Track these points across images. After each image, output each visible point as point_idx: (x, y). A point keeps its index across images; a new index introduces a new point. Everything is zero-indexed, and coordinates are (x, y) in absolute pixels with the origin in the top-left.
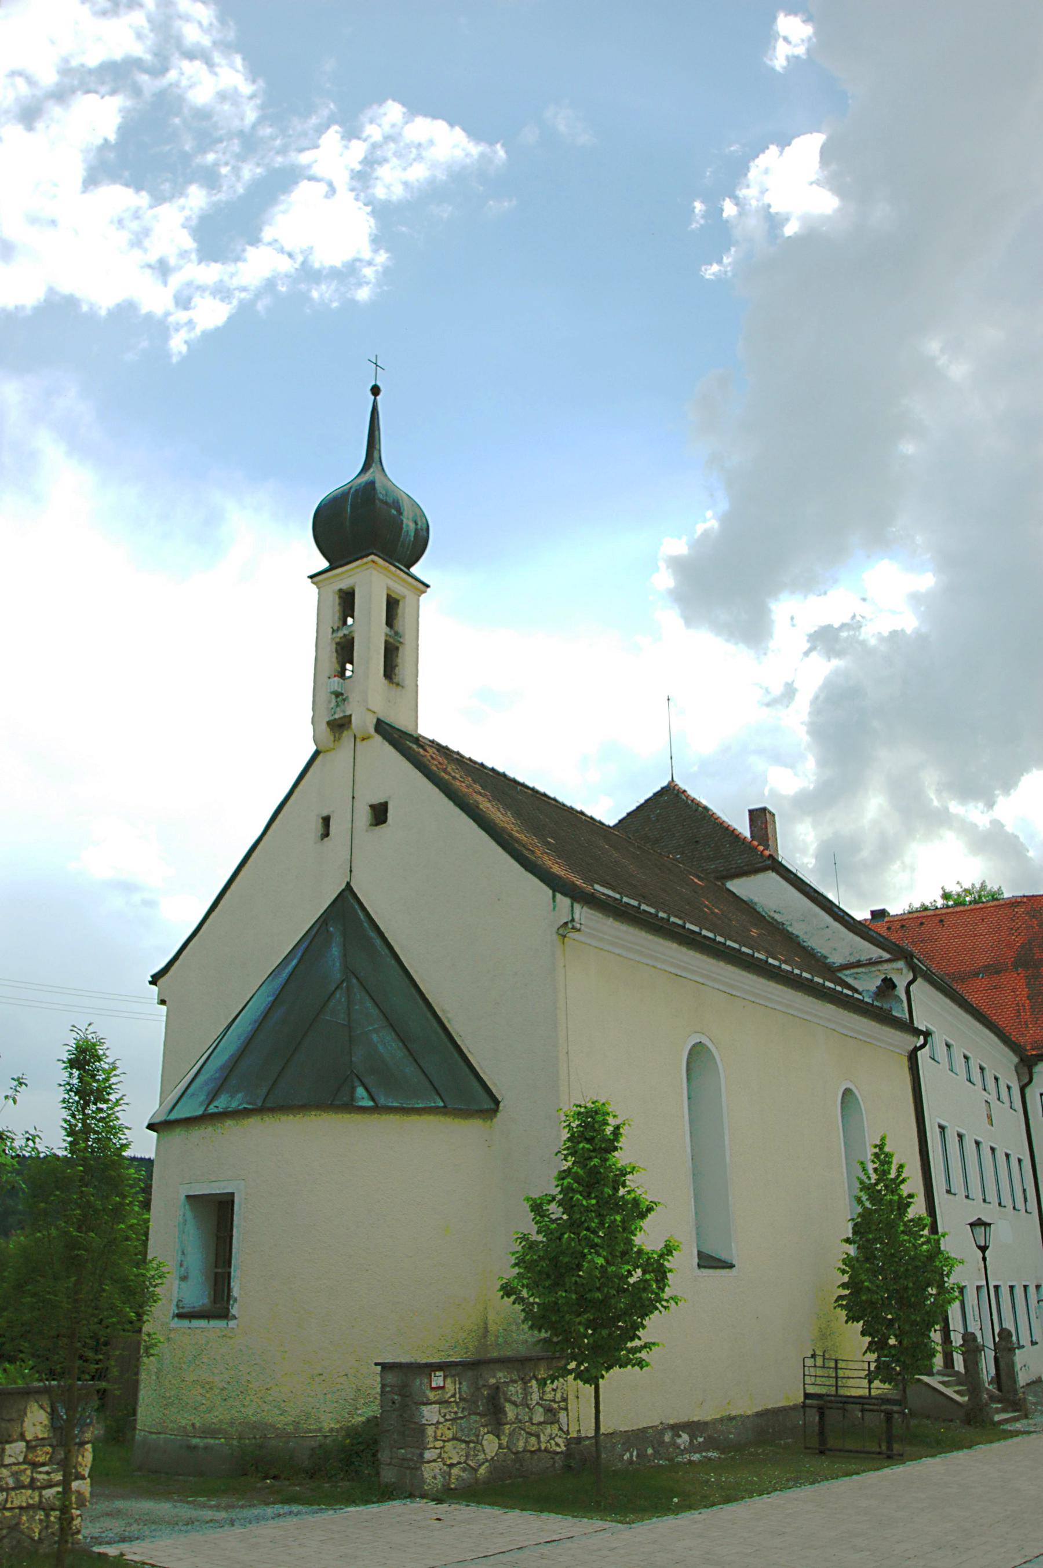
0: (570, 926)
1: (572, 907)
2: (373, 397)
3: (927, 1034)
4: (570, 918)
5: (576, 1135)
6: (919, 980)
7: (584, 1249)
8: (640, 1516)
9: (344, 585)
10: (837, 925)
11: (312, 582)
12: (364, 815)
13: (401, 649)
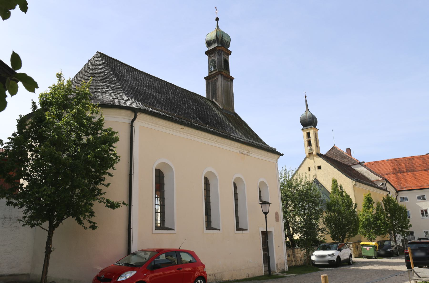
3: (389, 192)
8: (271, 273)
9: (308, 131)
10: (372, 173)
12: (317, 168)
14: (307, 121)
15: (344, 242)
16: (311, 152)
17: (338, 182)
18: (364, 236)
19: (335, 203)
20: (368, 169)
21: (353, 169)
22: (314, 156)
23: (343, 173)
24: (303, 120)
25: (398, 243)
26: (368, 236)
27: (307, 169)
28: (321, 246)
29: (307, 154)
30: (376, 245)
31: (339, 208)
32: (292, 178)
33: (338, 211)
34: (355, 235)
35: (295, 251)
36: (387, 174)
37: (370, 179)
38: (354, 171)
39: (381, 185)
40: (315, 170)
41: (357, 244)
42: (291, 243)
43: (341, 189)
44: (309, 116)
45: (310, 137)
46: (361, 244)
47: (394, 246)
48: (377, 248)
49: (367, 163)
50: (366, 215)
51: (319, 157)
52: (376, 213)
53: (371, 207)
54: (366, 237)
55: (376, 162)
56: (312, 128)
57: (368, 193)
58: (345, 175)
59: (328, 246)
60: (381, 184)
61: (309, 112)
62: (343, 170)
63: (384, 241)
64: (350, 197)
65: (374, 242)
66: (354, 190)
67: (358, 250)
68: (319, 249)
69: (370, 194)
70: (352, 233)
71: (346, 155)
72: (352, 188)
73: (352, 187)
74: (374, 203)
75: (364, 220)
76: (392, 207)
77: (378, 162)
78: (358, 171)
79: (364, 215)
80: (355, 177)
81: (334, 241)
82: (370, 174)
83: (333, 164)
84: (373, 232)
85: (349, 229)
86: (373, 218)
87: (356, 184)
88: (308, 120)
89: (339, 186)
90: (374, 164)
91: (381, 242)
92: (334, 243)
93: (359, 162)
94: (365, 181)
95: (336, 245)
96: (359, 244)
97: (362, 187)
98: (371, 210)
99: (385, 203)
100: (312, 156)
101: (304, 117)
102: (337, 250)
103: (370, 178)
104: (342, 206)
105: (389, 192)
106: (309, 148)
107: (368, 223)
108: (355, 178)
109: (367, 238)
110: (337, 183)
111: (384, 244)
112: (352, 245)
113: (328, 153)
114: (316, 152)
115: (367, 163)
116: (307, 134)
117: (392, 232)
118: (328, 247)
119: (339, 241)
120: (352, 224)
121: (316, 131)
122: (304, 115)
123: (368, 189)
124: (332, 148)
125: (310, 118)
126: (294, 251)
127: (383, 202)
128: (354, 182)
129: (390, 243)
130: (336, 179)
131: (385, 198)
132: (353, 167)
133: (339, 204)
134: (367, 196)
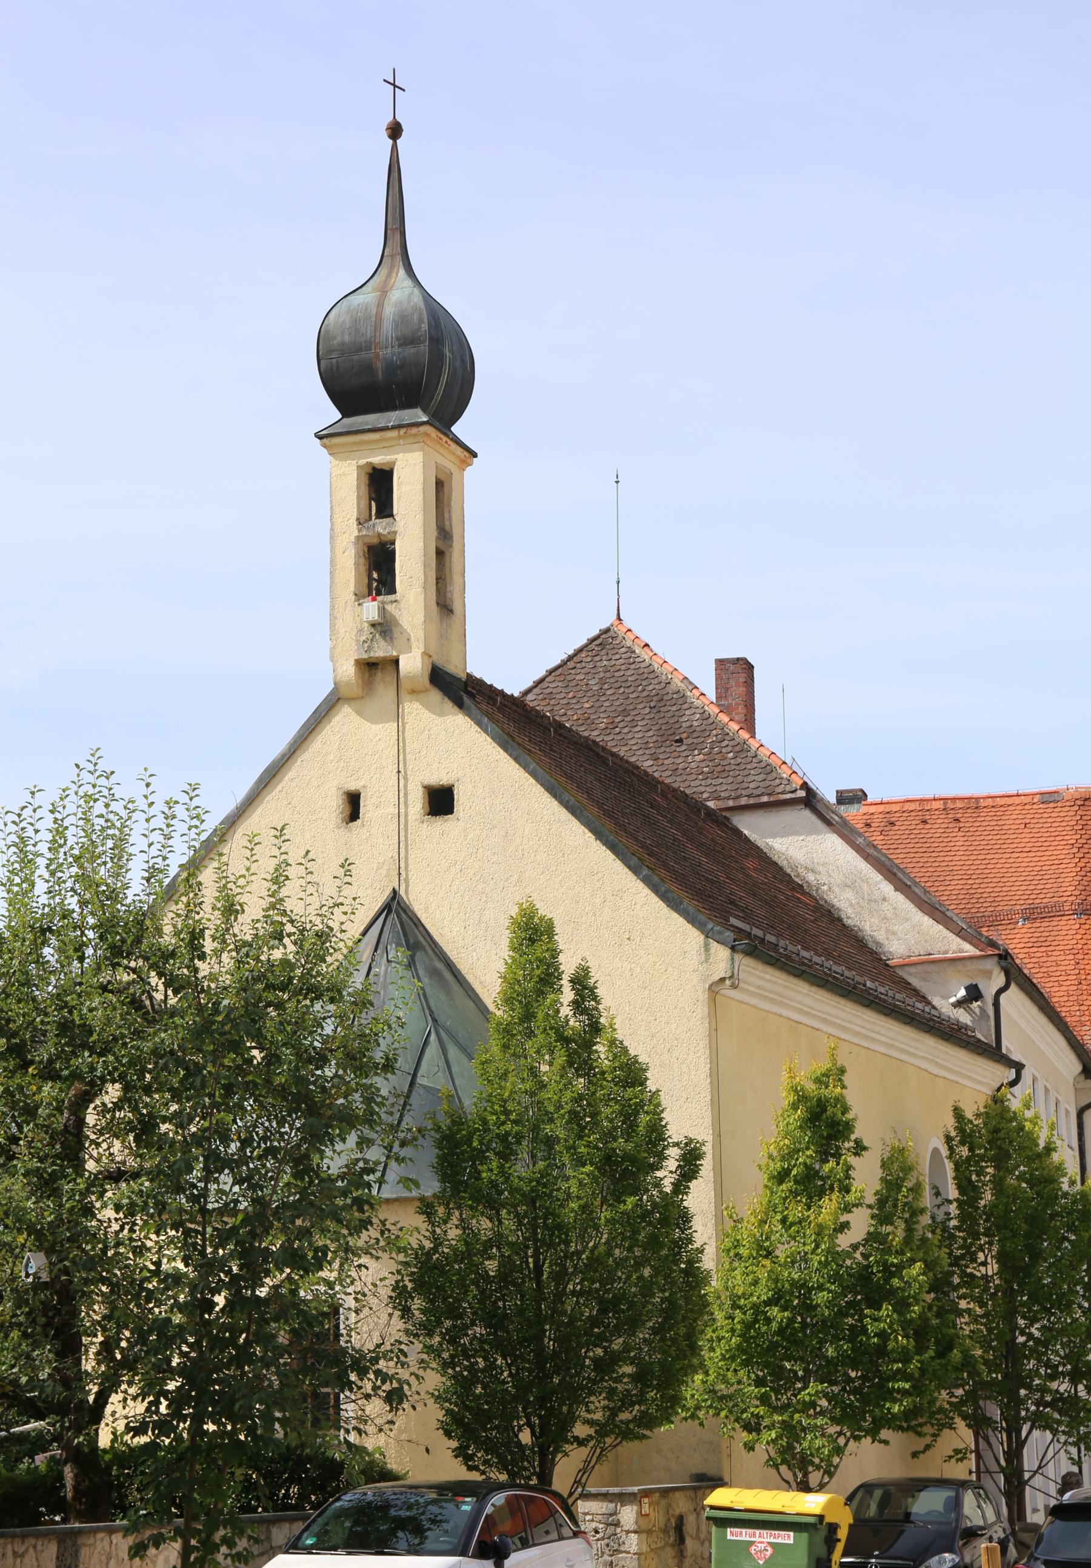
0: (728, 982)
1: (732, 959)
2: (391, 142)
4: (729, 974)
5: (848, 1262)
6: (1013, 988)
7: (150, 1362)
9: (379, 459)
11: (325, 446)
12: (417, 802)
13: (447, 555)
14: (379, 366)
15: (550, 1484)
16: (381, 650)
17: (561, 939)
18: (745, 1436)
19: (508, 1127)
20: (867, 857)
21: (747, 840)
22: (404, 695)
23: (635, 871)
24: (346, 350)
25: (1035, 1510)
26: (779, 1437)
27: (335, 804)
28: (344, 1513)
29: (348, 670)
30: (828, 1519)
31: (544, 1174)
32: (193, 866)
33: (531, 1200)
34: (648, 1421)
35: (84, 1552)
36: (1032, 914)
37: (878, 943)
38: (750, 864)
39: (959, 1004)
40: (400, 817)
41: (681, 1504)
42: (76, 1476)
43: (578, 1006)
44: (402, 318)
45: (391, 515)
46: (712, 1507)
47: (982, 1528)
48: (840, 1547)
49: (888, 808)
50: (781, 1252)
51: (449, 705)
52: (872, 1237)
53: (832, 1189)
54: (760, 1448)
55: (959, 804)
56: (414, 430)
57: (825, 1065)
58: (655, 889)
59: (404, 1514)
60: (962, 992)
61: (408, 283)
62: (643, 846)
63: (919, 1485)
64: (651, 1086)
65: (821, 1488)
66: (714, 1031)
67: (681, 1554)
68: (309, 1542)
69: (842, 1071)
70: (627, 1401)
71: (705, 716)
72: (702, 1010)
73: (703, 996)
74: (860, 1148)
75: (763, 1293)
76: (1016, 1193)
77: (974, 804)
78: (783, 863)
79: (769, 1254)
80: (743, 919)
81: (470, 1468)
82: (884, 899)
83: (570, 777)
84: (824, 1403)
85: (605, 1366)
86: (835, 1278)
87: (732, 980)
88: (389, 352)
89: (565, 982)
90: (940, 823)
91: (893, 1489)
92: (459, 1489)
93: (805, 786)
94: (829, 955)
95: (467, 1505)
96: (699, 1509)
97: (785, 1005)
98: (829, 1205)
99: (968, 1159)
100: (385, 693)
101: (356, 322)
102: (463, 1553)
103: (880, 936)
104: (566, 1159)
105: (1019, 1067)
106: (371, 609)
107: (791, 1320)
108: (734, 921)
109: (773, 1454)
110: (555, 953)
111: (908, 1515)
112: (635, 1508)
113: (551, 685)
114: (426, 654)
115: (881, 808)
116: (365, 479)
117: (994, 1411)
118: (401, 1524)
119: (512, 1475)
120: (633, 1323)
121: (448, 464)
122: (358, 299)
123: (800, 1011)
124: (592, 640)
125: (407, 341)
126: (76, 1555)
127: (951, 1149)
128: (721, 954)
129: (956, 1504)
130: (544, 910)
131: (969, 1114)
132: (751, 826)
133: (550, 1142)
134: (811, 1087)
